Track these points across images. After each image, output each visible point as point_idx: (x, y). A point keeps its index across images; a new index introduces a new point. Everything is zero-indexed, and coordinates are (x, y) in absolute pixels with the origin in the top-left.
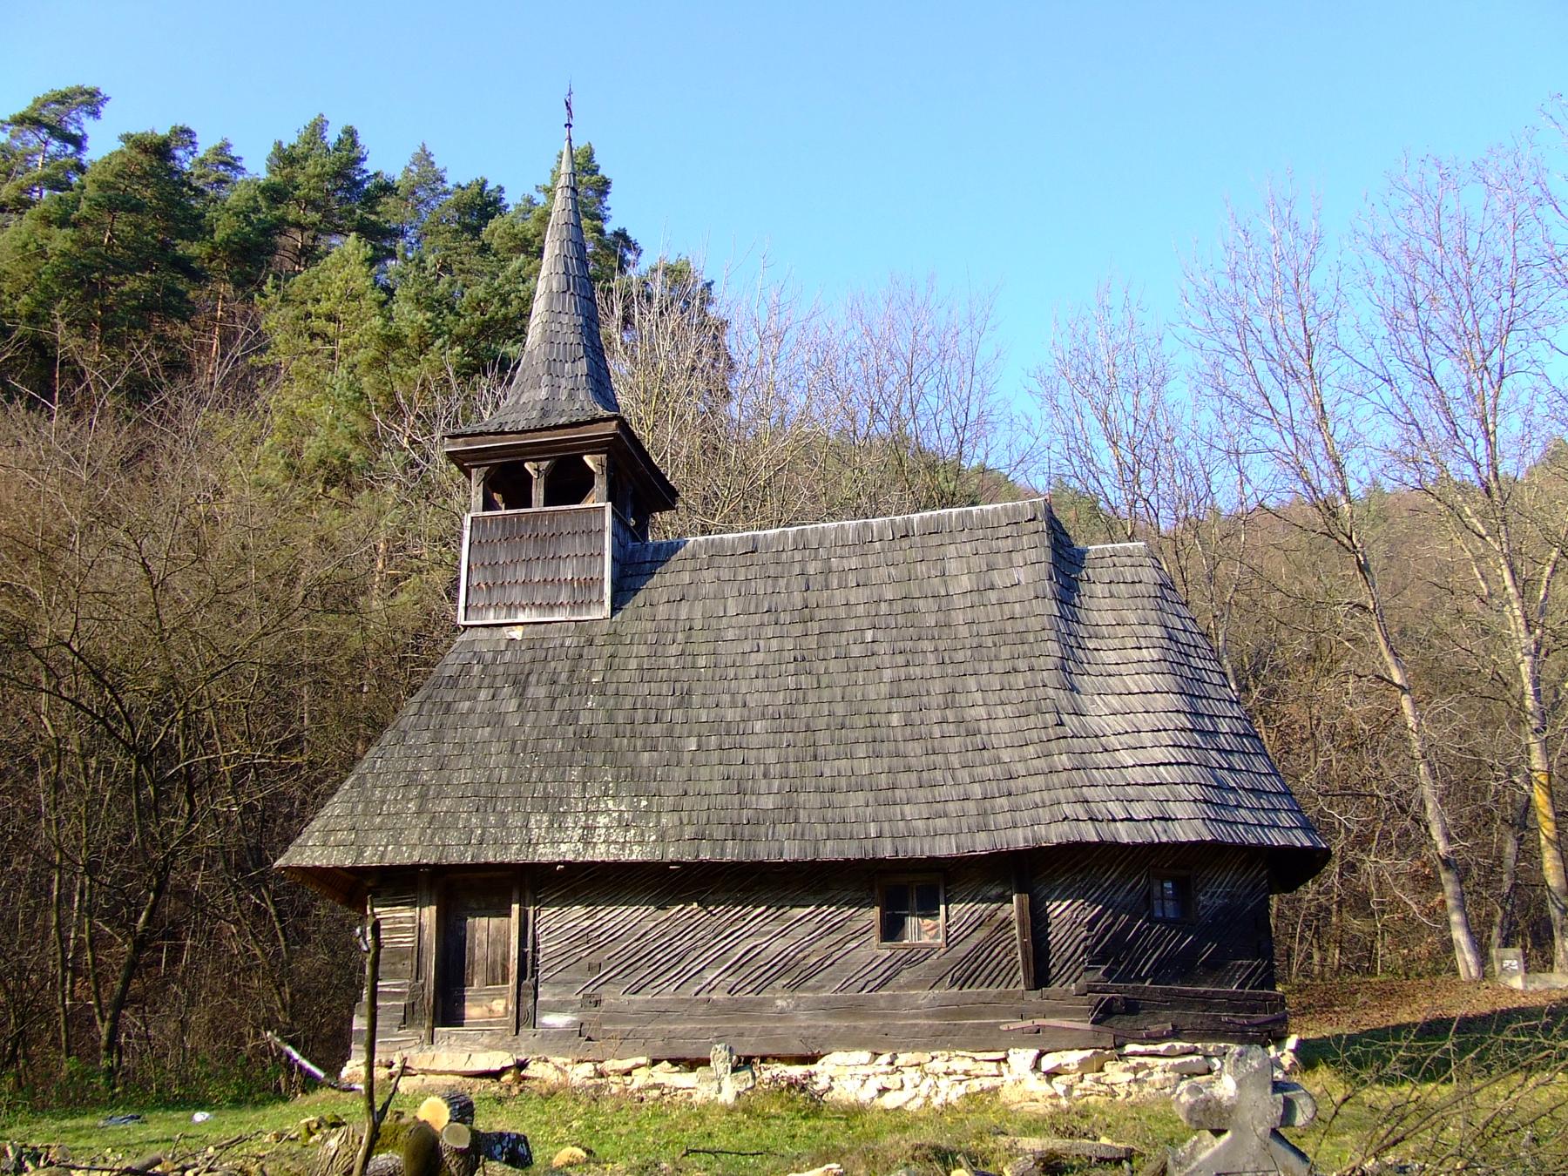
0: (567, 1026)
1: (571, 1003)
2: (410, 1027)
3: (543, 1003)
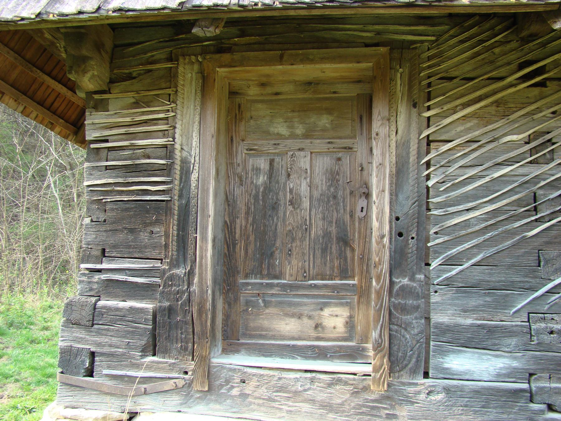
0: (500, 377)
1: (509, 332)
2: (166, 352)
3: (438, 326)
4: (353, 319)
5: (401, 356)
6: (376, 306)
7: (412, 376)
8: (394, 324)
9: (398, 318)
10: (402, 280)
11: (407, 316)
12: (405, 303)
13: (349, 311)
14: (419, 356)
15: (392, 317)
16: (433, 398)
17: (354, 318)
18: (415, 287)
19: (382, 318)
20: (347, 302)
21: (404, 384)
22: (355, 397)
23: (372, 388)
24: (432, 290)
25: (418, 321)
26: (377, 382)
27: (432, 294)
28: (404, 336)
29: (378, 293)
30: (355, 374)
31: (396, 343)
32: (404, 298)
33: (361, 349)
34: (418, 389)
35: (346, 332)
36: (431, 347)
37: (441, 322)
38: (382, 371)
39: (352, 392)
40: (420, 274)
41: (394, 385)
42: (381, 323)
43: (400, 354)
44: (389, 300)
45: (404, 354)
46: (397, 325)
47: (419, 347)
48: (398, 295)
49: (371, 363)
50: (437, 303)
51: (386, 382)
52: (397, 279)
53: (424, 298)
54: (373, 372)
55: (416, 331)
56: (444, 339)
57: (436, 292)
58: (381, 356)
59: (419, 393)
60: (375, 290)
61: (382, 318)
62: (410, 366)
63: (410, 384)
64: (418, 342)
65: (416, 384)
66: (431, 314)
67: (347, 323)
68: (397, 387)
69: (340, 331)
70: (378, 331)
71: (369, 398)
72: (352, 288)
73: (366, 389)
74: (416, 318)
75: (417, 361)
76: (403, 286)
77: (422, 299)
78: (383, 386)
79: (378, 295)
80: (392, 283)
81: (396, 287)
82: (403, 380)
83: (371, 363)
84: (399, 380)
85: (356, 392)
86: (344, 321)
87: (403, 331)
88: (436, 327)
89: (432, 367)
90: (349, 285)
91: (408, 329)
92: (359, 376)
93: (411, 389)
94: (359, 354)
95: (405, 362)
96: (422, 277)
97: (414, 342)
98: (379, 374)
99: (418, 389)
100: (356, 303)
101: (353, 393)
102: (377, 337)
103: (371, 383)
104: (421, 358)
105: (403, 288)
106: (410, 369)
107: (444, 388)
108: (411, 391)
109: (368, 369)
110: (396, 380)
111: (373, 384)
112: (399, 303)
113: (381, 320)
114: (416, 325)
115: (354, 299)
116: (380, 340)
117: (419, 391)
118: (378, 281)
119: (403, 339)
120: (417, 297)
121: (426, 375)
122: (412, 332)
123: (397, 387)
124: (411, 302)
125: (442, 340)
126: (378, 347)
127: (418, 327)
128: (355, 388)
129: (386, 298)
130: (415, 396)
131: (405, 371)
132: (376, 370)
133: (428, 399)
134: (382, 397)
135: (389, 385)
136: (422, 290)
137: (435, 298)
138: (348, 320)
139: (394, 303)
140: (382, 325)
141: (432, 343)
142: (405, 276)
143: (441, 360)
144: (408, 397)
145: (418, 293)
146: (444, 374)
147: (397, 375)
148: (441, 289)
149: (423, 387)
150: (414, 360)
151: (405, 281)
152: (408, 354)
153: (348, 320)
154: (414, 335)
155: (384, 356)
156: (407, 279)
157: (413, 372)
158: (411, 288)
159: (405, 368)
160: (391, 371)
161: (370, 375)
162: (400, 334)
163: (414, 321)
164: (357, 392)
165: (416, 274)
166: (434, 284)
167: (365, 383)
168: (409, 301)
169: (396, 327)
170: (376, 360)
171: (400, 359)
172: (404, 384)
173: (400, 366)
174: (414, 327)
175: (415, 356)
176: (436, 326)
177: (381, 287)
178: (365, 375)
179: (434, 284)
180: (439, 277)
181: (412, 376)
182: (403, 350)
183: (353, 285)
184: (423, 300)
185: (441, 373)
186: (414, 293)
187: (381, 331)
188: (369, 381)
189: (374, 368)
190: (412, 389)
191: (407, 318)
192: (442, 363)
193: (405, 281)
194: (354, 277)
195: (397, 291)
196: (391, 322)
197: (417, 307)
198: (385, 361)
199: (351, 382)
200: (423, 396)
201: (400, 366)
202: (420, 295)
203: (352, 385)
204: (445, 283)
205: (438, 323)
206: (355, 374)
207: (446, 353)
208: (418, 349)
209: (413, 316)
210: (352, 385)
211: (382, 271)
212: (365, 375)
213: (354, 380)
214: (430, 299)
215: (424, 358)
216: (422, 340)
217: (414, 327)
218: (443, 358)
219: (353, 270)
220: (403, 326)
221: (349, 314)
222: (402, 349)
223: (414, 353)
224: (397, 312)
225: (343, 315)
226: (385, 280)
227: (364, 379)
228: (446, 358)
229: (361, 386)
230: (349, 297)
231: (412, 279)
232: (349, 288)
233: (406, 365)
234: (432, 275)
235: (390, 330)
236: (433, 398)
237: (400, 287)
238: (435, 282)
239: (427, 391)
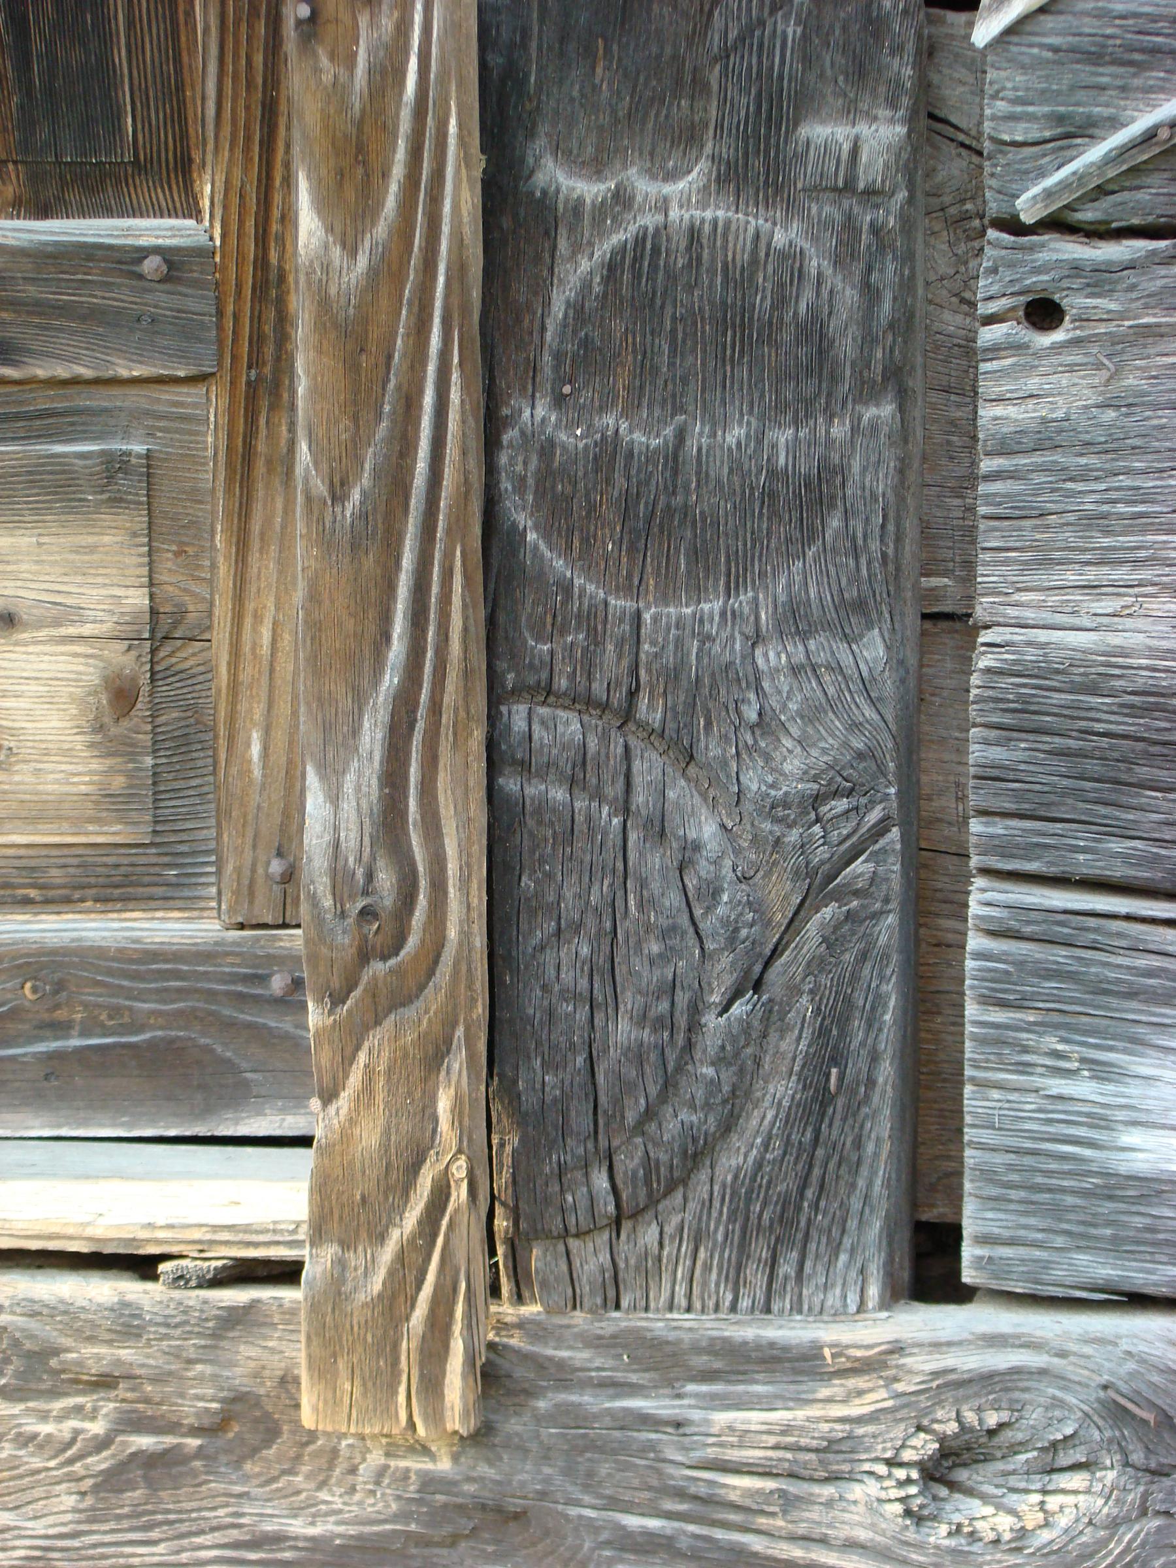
3: (1046, 702)
4: (187, 657)
5: (637, 1054)
6: (338, 494)
7: (756, 1277)
8: (546, 692)
9: (593, 621)
10: (644, 187)
11: (698, 592)
12: (674, 457)
13: (134, 561)
14: (829, 1049)
15: (528, 607)
16: (992, 1521)
17: (199, 636)
18: (791, 258)
19: (399, 627)
20: (116, 465)
21: (666, 1363)
22: (144, 1521)
23: (307, 1419)
24: (993, 290)
25: (821, 647)
26: (368, 1344)
27: (989, 335)
28: (658, 829)
29: (355, 339)
30: (143, 1266)
31: (570, 907)
32: (649, 389)
33: (278, 983)
34: (823, 1411)
35: (112, 803)
36: (975, 942)
37: (1081, 658)
38: (411, 1218)
39: (100, 1462)
40: (851, 112)
41: (565, 1376)
42: (390, 680)
43: (623, 1031)
44: (492, 425)
45: (666, 1023)
46: (581, 701)
47: (832, 941)
48: (586, 360)
49: (305, 1141)
50: (1045, 437)
51: (457, 1346)
52: (597, 167)
53: (895, 379)
54: (319, 1231)
55: (793, 766)
56: (1117, 855)
57: (1043, 313)
58: (399, 1060)
59: (834, 1459)
60: (324, 303)
61: (399, 627)
62: (735, 1159)
63: (739, 1363)
64: (819, 885)
65: (803, 1365)
66: (987, 576)
67: (122, 696)
68: (586, 1399)
69: (51, 786)
70: (363, 776)
71: (298, 1527)
72: (162, 301)
73: (249, 1424)
74: (796, 621)
75: (816, 1103)
76: (645, 252)
77: (867, 392)
78: (432, 1385)
79: (352, 367)
80: (514, 221)
81: (577, 271)
82: (656, 1324)
83: (305, 1141)
84: (617, 1321)
85: (150, 1461)
86: (91, 674)
87: (649, 766)
88: (1021, 721)
89: (987, 1175)
90: (125, 261)
91: (711, 748)
92: (180, 1280)
93: (749, 1423)
94: (258, 1033)
95: (677, 1121)
96: (878, 136)
97: (780, 894)
98: (387, 1254)
99: (823, 1411)
100: (211, 475)
101: (111, 1482)
102: (350, 839)
103: (297, 1353)
104: (857, 1066)
105: (643, 272)
106: (743, 1195)
107: (1116, 1412)
108: (744, 1437)
109: (267, 1198)
110: (579, 1318)
111: (323, 1371)
112: (608, 452)
113: (397, 649)
114: (787, 697)
115: (190, 420)
116: (386, 879)
117: (831, 1446)
118: (350, 204)
119: (654, 862)
120: (807, 371)
121: (930, 1267)
122: (752, 781)
123: (586, 1399)
124: (735, 434)
125: (1083, 864)
126: (364, 956)
127: (812, 714)
128: (134, 1423)
129: (447, 401)
130: (789, 1502)
131: (678, 1212)
132: (344, 1213)
133: (939, 1534)
134: (438, 1515)
135: (493, 1377)
136: (870, 293)
137: (1028, 389)
138: (119, 657)
139: (547, 449)
140: (405, 700)
141: (983, 899)
142: (689, 137)
143: (1084, 1088)
144: (708, 1505)
145: (814, 332)
146: (1116, 1247)
147: (592, 1257)
148: (1100, 278)
149: (877, 1398)
150: (779, 1090)
151: (677, 196)
152: (711, 1020)
153: (119, 657)
154: (774, 809)
155: (434, 1057)
156: (697, 175)
157: (778, 1232)
158: (741, 279)
159: (678, 1182)
160: (523, 1224)
161: (288, 1273)
162: (625, 809)
163: (770, 657)
164: (153, 1465)
165: (804, 104)
166: (1013, 226)
167: (248, 1360)
168: (718, 423)
169: (570, 725)
170: (344, 1102)
171: (624, 1088)
172: (666, 1363)
173: (629, 1162)
174: (764, 724)
175: (793, 1045)
176: (1025, 707)
177: (387, 271)
178: (246, 1273)
179: (1013, 226)
180: (1073, 132)
181: (756, 1277)
182: (651, 977)
183: (175, 262)
184: (884, 411)
185: (1084, 1241)
186: (771, 328)
187: (393, 777)
188: (282, 1340)
189: (323, 1189)
190: (754, 1418)
191: (684, 618)
192: (1100, 1121)
193: (677, 196)
194: (183, 169)
195: (578, 312)
196: (502, 676)
197: (812, 495)
198: (444, 1104)
199: (95, 1356)
200: (871, 1502)
201: (629, 1162)
202: (847, 347)
203: (104, 1382)
204: (1149, 199)
205: (1043, 672)
206: (143, 1266)
207: (1133, 1010)
208: (817, 965)
209: (760, 603)
210: (104, 1382)
211: (388, 74)
212: (246, 1273)
213: (127, 1324)
214: (972, 395)
215: (886, 1072)
216: (860, 866)
217: (764, 724)
218: (1102, 1072)
219: (174, 91)
220: (650, 711)
221: (138, 599)
222: (641, 970)
223: (772, 1016)
224: (584, 552)
225: (74, 614)
226: (423, 188)
227: (235, 1319)
228: (1143, 1065)
229: (198, 1400)
230: (135, 398)
231: (759, 165)
232: (122, 297)
233: (697, 1152)
234: (1003, 109)
235: (496, 757)
236: (992, 1521)
237: (612, 268)
238: (1029, 204)
239: (923, 1446)
